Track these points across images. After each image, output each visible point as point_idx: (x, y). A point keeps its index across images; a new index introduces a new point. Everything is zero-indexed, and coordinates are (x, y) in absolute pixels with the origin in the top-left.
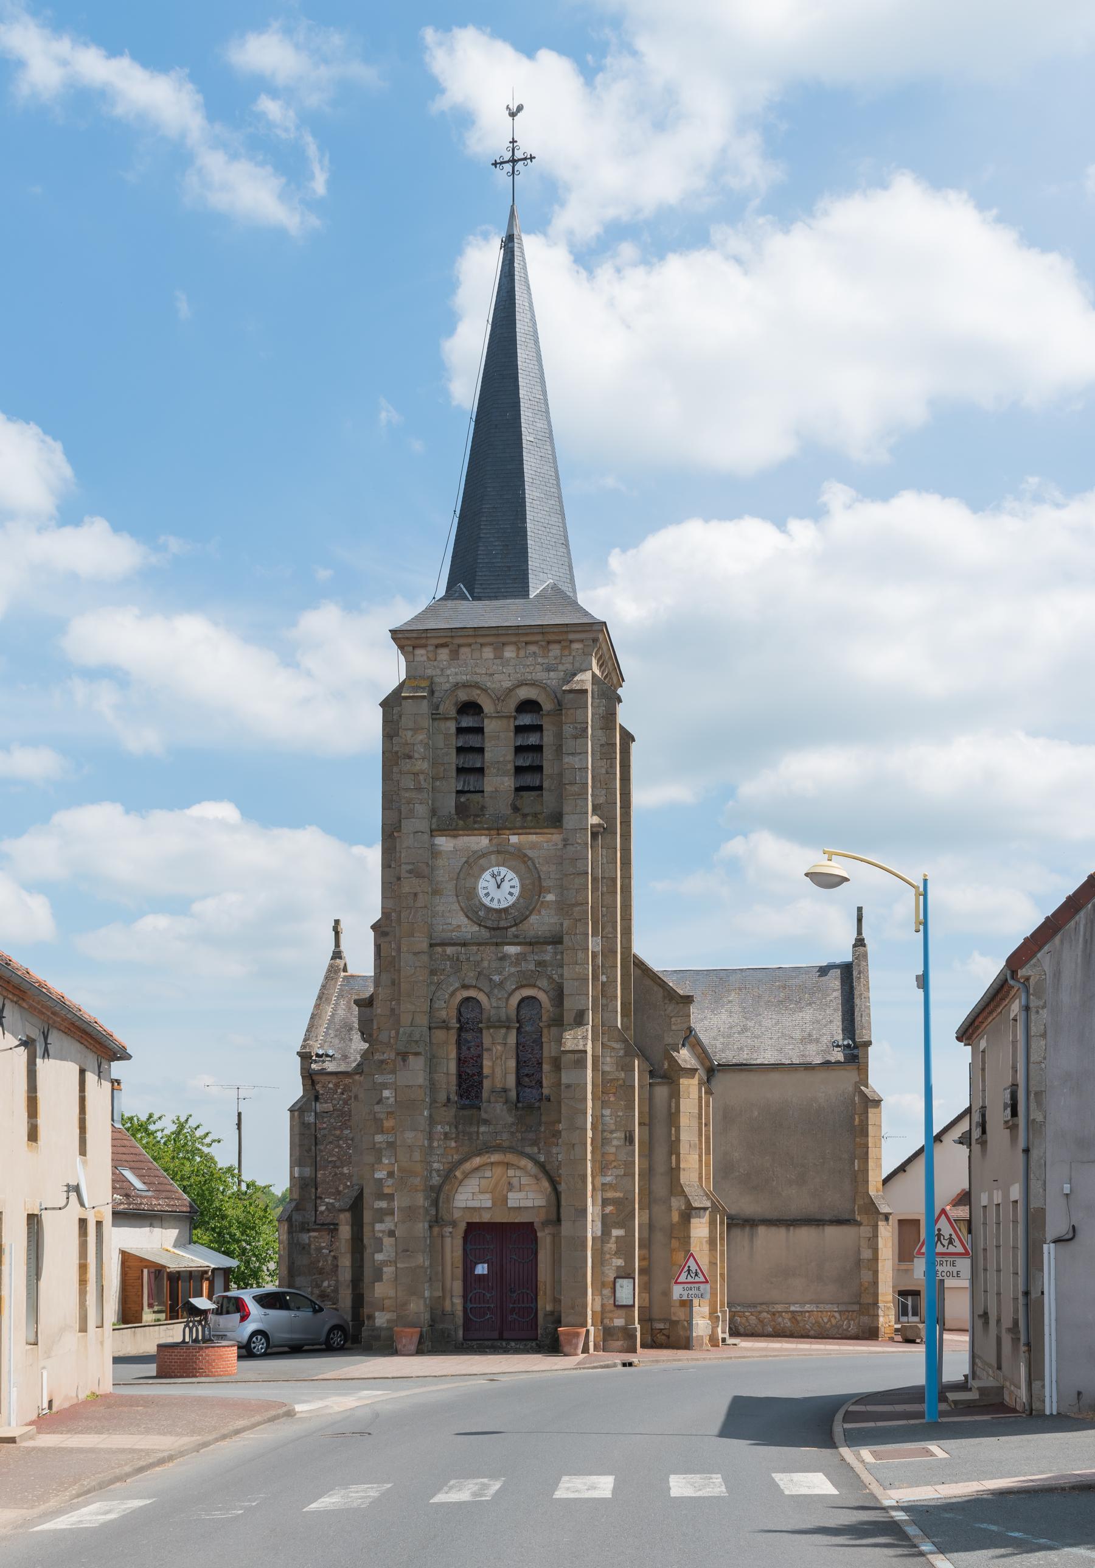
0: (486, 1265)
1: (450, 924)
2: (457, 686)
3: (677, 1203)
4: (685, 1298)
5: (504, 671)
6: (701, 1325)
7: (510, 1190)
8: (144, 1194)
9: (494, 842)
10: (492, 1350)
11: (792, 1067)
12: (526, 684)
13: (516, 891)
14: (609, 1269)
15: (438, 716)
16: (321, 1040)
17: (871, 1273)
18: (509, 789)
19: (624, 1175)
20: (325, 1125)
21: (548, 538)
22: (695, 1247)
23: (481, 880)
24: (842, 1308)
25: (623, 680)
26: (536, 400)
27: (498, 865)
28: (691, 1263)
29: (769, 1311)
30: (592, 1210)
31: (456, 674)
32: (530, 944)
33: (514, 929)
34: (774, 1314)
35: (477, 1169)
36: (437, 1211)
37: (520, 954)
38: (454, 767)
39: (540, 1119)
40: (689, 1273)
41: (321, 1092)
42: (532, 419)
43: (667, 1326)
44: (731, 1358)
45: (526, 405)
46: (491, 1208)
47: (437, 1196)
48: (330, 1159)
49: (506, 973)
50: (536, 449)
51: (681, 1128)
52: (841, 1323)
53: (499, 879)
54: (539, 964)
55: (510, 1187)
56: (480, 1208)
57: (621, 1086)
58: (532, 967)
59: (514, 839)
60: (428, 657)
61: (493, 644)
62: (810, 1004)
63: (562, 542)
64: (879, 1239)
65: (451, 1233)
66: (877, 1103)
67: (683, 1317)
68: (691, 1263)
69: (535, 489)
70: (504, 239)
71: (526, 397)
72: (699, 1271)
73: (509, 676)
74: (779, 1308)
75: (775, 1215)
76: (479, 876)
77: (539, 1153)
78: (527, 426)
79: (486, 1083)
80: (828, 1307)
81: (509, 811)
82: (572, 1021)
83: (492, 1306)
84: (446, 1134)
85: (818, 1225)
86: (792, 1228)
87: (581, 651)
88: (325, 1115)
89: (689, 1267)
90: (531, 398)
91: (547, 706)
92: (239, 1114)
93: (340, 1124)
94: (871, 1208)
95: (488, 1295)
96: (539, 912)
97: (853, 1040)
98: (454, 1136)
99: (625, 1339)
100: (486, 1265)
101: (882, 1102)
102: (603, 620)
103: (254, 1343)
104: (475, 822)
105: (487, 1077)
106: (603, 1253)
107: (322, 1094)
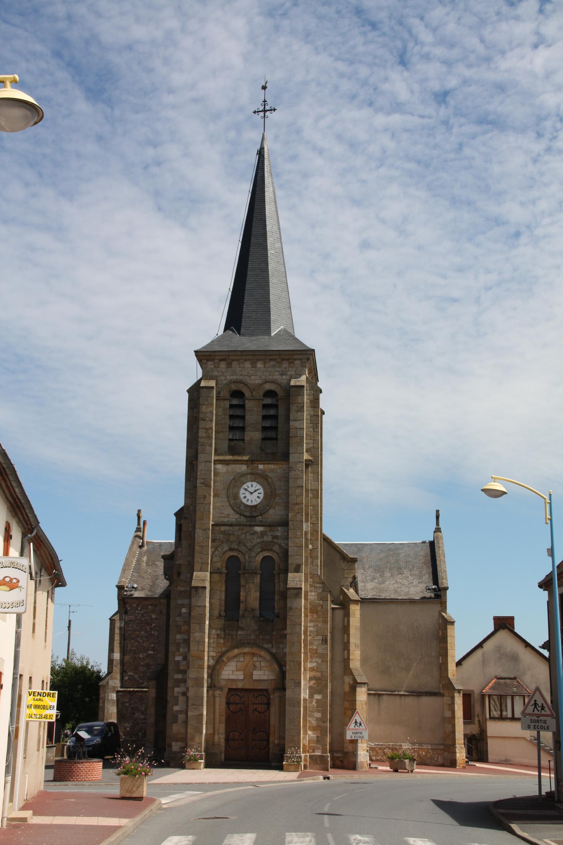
3: (348, 680)
4: (353, 738)
6: (363, 756)
7: (254, 669)
9: (250, 468)
12: (269, 382)
13: (262, 496)
15: (220, 398)
16: (129, 578)
17: (451, 726)
18: (258, 438)
20: (130, 629)
21: (281, 304)
24: (434, 747)
26: (275, 232)
30: (304, 683)
32: (269, 526)
33: (260, 517)
35: (235, 656)
37: (264, 531)
38: (228, 426)
41: (129, 609)
42: (273, 242)
43: (341, 755)
45: (270, 235)
46: (242, 680)
47: (212, 672)
48: (132, 649)
50: (275, 257)
51: (351, 635)
55: (255, 667)
56: (236, 680)
59: (261, 467)
61: (251, 360)
63: (288, 306)
64: (456, 705)
65: (219, 694)
66: (452, 623)
69: (274, 278)
70: (259, 150)
71: (270, 231)
77: (272, 647)
78: (270, 245)
79: (242, 606)
84: (218, 635)
88: (130, 622)
91: (280, 393)
92: (70, 622)
93: (139, 628)
94: (449, 686)
96: (274, 507)
97: (438, 586)
98: (223, 636)
101: (455, 623)
102: (313, 348)
107: (129, 610)
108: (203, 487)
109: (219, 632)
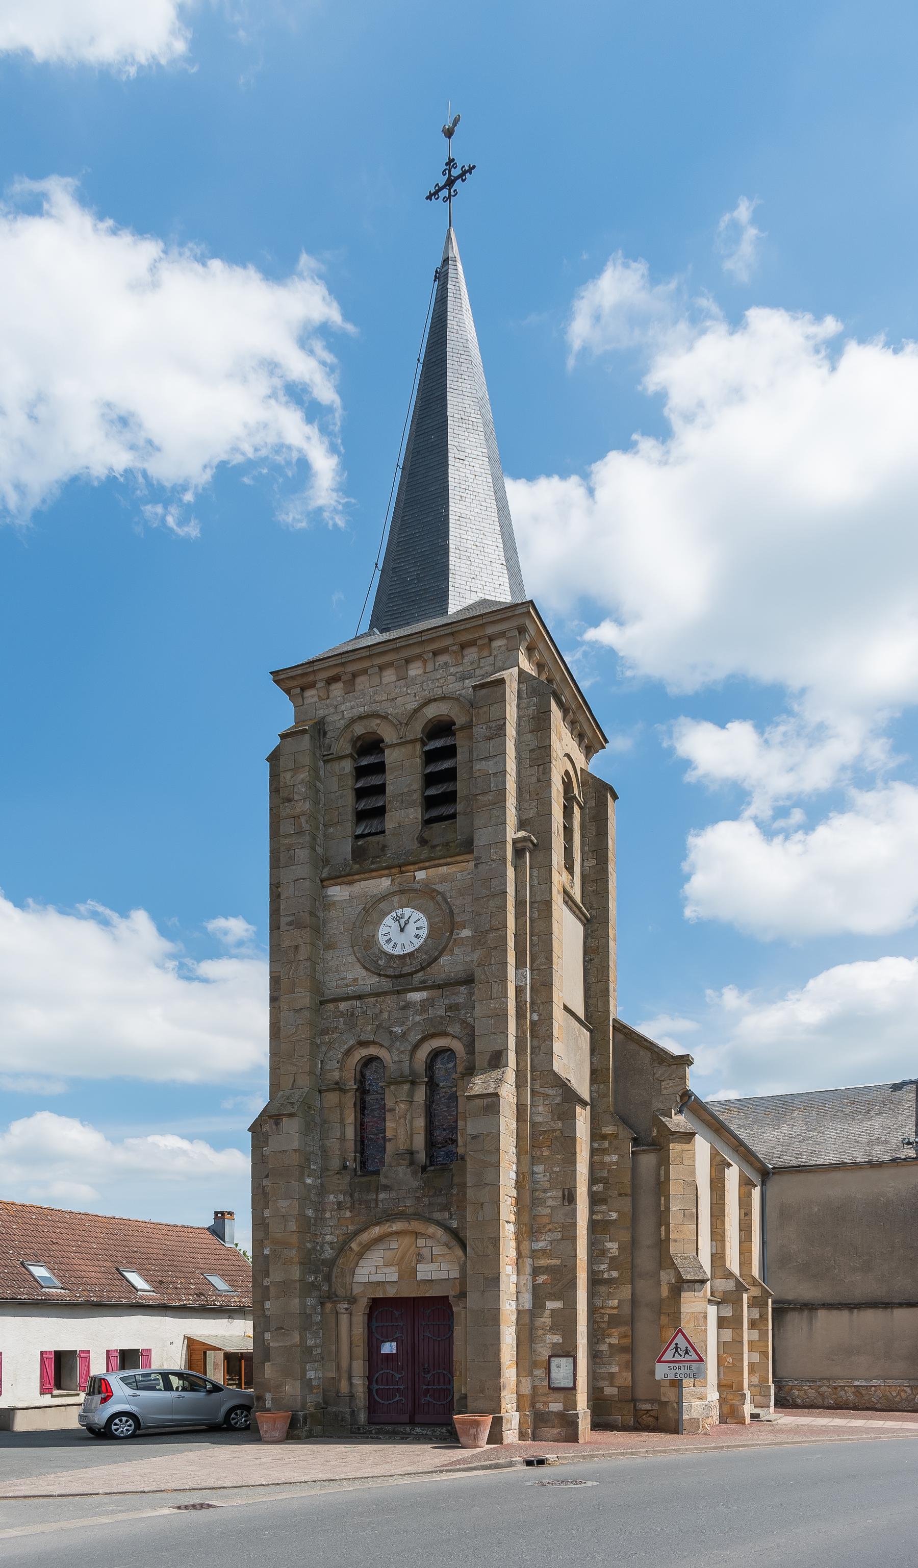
0: (394, 1344)
1: (346, 978)
2: (353, 721)
5: (409, 691)
7: (420, 1262)
8: (232, 1294)
9: (397, 881)
10: (387, 1436)
11: (855, 1166)
12: (435, 700)
13: (424, 933)
14: (542, 1347)
15: (330, 757)
18: (415, 821)
19: (562, 1239)
22: (688, 1322)
23: (382, 925)
25: (606, 741)
27: (402, 907)
28: (680, 1339)
29: (830, 1385)
31: (352, 708)
32: (439, 987)
33: (420, 974)
34: (835, 1388)
36: (330, 1286)
37: (427, 999)
39: (452, 1180)
40: (677, 1351)
44: (722, 1447)
49: (409, 1023)
52: (912, 1396)
53: (402, 921)
54: (450, 1008)
55: (420, 1258)
57: (557, 1137)
58: (441, 1012)
59: (421, 875)
60: (319, 696)
62: (880, 1114)
65: (346, 1309)
67: (673, 1398)
68: (680, 1339)
72: (690, 1348)
73: (415, 696)
74: (841, 1382)
75: (838, 1300)
76: (380, 922)
79: (389, 1147)
80: (896, 1382)
81: (415, 845)
82: (486, 1064)
83: (402, 1387)
84: (339, 1203)
85: (886, 1308)
86: (855, 1311)
87: (504, 648)
89: (677, 1344)
90: (463, 417)
91: (460, 720)
95: (397, 1376)
96: (452, 951)
98: (348, 1205)
99: (562, 1427)
100: (394, 1344)
103: (121, 1421)
104: (373, 863)
105: (390, 1140)
106: (532, 1328)
108: (293, 931)
109: (341, 1197)
